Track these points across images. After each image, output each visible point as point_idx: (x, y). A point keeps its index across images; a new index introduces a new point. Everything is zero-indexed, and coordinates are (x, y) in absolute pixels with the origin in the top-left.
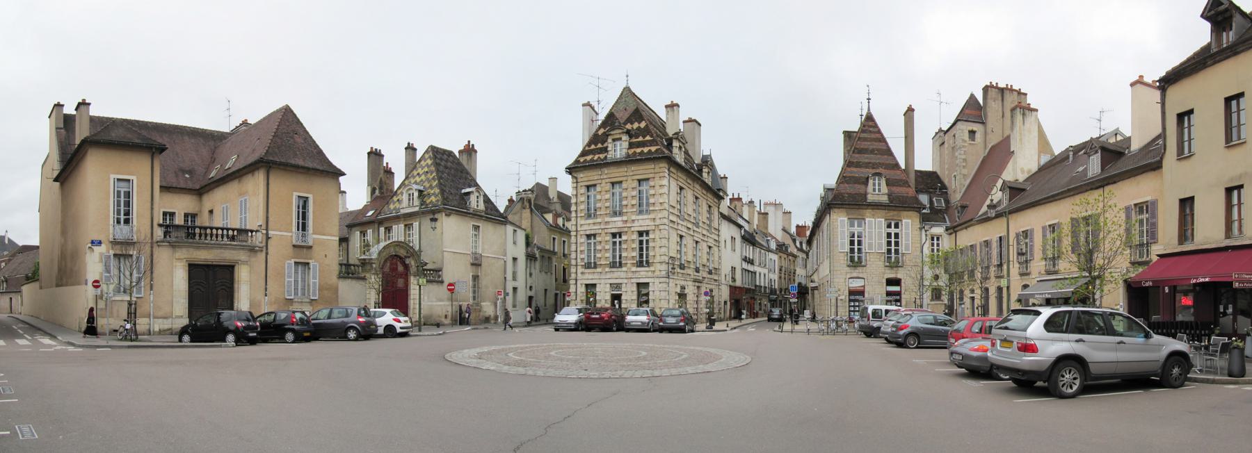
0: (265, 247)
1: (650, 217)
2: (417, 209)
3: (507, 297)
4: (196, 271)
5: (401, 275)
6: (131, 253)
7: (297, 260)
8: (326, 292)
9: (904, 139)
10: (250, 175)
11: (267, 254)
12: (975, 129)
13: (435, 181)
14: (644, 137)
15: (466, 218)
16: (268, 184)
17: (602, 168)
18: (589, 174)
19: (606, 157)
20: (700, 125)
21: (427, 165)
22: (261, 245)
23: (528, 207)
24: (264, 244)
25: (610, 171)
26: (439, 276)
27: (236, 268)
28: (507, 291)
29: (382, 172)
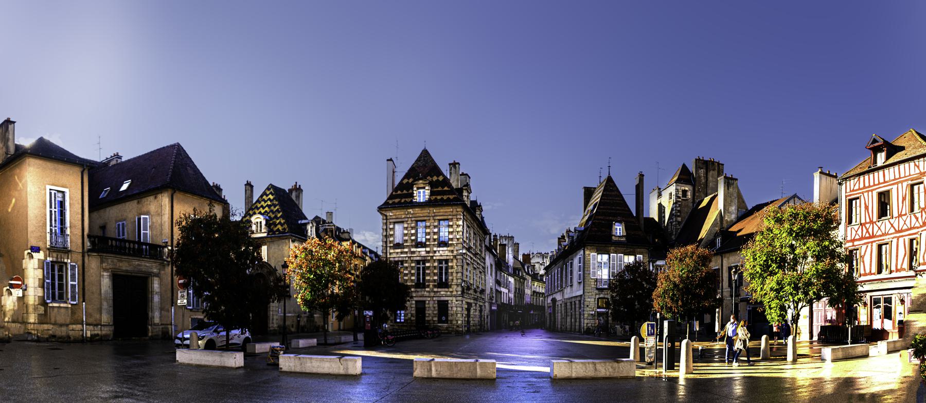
1: (449, 249)
4: (118, 279)
6: (66, 261)
9: (635, 196)
10: (152, 198)
12: (687, 189)
13: (279, 213)
14: (443, 187)
20: (470, 178)
21: (269, 199)
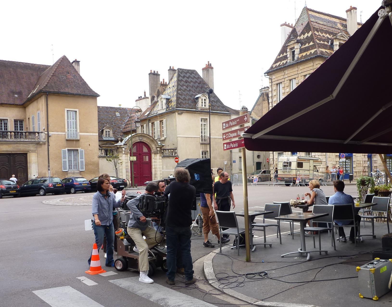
0: (47, 142)
2: (165, 111)
3: (233, 164)
5: (146, 154)
7: (69, 148)
8: (90, 166)
11: (49, 145)
14: (309, 43)
15: (196, 114)
16: (47, 105)
17: (284, 70)
18: (278, 76)
19: (287, 62)
22: (44, 141)
23: (266, 99)
24: (46, 140)
25: (289, 72)
26: (176, 153)
27: (28, 155)
28: (233, 159)
29: (159, 85)
